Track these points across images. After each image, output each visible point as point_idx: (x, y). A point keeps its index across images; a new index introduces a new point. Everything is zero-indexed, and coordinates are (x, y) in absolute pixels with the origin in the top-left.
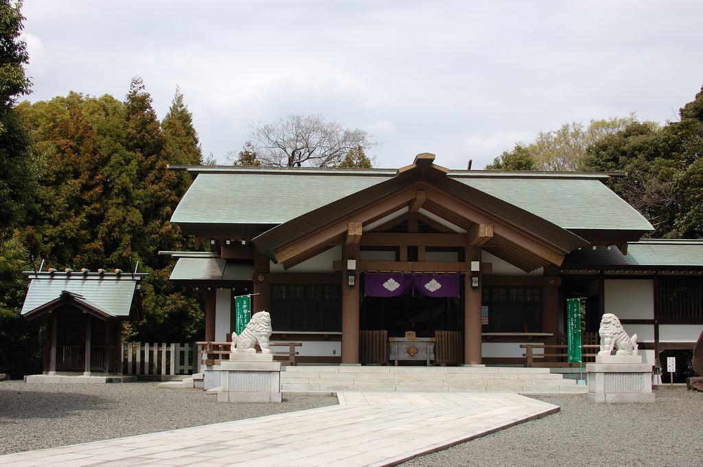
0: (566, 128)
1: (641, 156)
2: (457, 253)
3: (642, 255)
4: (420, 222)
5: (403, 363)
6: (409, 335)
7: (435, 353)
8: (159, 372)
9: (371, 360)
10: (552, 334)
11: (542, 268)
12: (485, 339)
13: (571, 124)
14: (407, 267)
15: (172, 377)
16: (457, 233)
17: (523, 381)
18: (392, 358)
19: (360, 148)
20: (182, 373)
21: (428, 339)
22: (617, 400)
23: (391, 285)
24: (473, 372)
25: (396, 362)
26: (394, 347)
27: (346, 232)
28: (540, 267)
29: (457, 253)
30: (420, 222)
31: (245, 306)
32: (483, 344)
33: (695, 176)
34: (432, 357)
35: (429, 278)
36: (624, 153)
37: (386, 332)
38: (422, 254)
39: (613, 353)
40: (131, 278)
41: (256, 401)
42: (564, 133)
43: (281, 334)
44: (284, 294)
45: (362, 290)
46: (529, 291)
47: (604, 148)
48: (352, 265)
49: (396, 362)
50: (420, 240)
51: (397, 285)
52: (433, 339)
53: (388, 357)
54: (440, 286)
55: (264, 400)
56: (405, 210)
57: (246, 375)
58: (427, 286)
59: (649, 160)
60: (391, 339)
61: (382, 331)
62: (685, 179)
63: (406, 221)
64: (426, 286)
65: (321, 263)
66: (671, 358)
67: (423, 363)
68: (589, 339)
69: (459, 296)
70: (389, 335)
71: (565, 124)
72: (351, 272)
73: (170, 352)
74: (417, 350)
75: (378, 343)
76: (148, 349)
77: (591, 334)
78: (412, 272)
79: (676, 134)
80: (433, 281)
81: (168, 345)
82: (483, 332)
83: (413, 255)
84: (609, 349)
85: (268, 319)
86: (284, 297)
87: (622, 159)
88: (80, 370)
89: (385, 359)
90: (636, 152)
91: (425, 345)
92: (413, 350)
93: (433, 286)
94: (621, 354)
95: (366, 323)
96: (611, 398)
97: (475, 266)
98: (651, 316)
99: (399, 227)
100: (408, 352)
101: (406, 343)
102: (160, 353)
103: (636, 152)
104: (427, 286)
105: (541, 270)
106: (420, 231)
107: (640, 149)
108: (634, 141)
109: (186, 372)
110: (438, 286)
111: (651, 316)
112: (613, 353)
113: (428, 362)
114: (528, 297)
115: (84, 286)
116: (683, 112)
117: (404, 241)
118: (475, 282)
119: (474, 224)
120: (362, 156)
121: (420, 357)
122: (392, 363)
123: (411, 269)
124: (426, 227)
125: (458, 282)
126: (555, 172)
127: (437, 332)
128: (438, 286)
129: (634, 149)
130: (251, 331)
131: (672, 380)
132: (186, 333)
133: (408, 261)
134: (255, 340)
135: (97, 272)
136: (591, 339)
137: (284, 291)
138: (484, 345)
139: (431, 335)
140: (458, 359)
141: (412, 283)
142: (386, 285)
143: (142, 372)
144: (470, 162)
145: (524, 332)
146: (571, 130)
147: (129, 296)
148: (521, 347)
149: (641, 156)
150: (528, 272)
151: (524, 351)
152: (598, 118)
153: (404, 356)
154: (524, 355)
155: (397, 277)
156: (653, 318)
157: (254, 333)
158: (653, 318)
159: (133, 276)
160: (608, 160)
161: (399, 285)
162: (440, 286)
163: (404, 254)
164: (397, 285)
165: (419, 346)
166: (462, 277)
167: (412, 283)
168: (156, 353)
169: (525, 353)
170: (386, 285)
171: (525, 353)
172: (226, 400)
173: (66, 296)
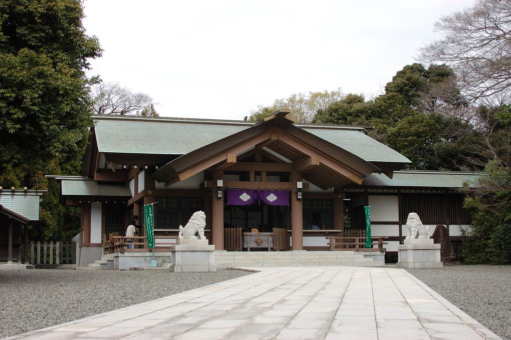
0: (294, 96)
1: (363, 117)
2: (279, 177)
3: (400, 180)
5: (252, 250)
6: (254, 231)
7: (273, 243)
8: (54, 263)
9: (229, 248)
10: (341, 231)
11: (333, 188)
12: (305, 234)
13: (298, 94)
15: (57, 265)
16: (286, 163)
18: (245, 246)
19: (152, 105)
20: (65, 262)
21: (269, 233)
22: (421, 266)
23: (245, 197)
24: (298, 254)
25: (249, 249)
26: (247, 239)
29: (279, 177)
31: (150, 211)
32: (304, 238)
33: (404, 130)
34: (272, 245)
35: (269, 192)
36: (350, 114)
37: (241, 229)
39: (417, 237)
40: (35, 194)
41: (200, 271)
43: (164, 231)
45: (225, 201)
47: (336, 111)
49: (249, 249)
51: (249, 197)
52: (272, 233)
53: (243, 245)
54: (276, 198)
55: (205, 271)
57: (192, 253)
58: (268, 198)
59: (368, 120)
60: (245, 233)
61: (238, 229)
62: (397, 132)
67: (265, 249)
68: (353, 233)
69: (288, 205)
70: (243, 231)
71: (293, 94)
73: (55, 247)
74: (262, 241)
75: (235, 237)
76: (40, 246)
77: (361, 230)
78: (258, 189)
79: (386, 102)
80: (272, 195)
81: (55, 243)
82: (303, 229)
84: (414, 235)
85: (205, 216)
86: (164, 206)
87: (349, 118)
89: (241, 247)
90: (360, 114)
92: (259, 242)
93: (272, 198)
94: (421, 238)
96: (417, 265)
97: (300, 185)
98: (397, 220)
100: (256, 242)
101: (254, 236)
102: (48, 248)
103: (360, 114)
104: (268, 198)
107: (362, 112)
108: (357, 106)
109: (68, 262)
110: (275, 198)
111: (397, 220)
112: (417, 237)
113: (269, 249)
114: (324, 207)
116: (387, 89)
120: (153, 112)
121: (264, 245)
122: (245, 250)
125: (286, 195)
127: (274, 229)
128: (275, 198)
129: (358, 111)
132: (45, 236)
136: (355, 233)
137: (164, 202)
138: (305, 238)
139: (271, 231)
140: (287, 247)
142: (241, 197)
143: (48, 262)
145: (333, 229)
146: (298, 98)
147: (36, 206)
149: (363, 117)
150: (325, 190)
151: (328, 241)
152: (315, 91)
153: (254, 245)
154: (328, 244)
155: (276, 192)
156: (398, 221)
158: (398, 221)
159: (37, 192)
160: (339, 119)
162: (276, 198)
164: (249, 197)
165: (263, 238)
166: (290, 192)
168: (45, 248)
169: (329, 242)
170: (241, 197)
171: (329, 242)
172: (180, 271)
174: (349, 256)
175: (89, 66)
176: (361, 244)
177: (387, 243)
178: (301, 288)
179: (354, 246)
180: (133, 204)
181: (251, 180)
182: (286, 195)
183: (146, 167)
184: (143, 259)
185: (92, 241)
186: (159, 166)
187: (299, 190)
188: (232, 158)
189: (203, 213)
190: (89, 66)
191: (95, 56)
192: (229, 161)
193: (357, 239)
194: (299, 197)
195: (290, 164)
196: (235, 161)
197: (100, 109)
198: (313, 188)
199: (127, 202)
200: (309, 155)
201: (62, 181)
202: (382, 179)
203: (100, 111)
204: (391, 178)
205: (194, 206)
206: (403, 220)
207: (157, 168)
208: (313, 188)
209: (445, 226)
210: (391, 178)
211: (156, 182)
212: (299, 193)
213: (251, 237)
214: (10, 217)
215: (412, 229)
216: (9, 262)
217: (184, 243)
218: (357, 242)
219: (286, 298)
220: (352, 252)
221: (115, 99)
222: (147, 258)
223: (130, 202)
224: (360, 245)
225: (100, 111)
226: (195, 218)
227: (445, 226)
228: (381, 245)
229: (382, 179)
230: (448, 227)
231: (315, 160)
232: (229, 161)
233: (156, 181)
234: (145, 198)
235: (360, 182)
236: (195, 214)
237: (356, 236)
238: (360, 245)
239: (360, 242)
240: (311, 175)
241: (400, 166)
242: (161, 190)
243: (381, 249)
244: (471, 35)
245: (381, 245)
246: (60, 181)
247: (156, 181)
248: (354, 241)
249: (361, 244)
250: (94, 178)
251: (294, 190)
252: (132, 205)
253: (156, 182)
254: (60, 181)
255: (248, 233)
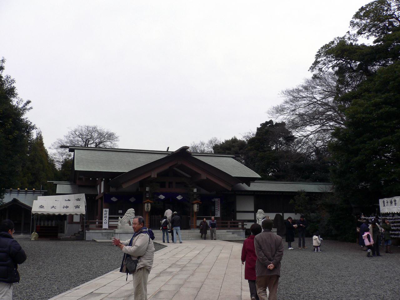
3: (254, 187)
27: (151, 176)
32: (197, 221)
42: (44, 144)
72: (147, 192)
85: (134, 212)
93: (179, 198)
97: (195, 190)
98: (253, 209)
115: (19, 196)
118: (148, 195)
119: (199, 174)
126: (202, 153)
130: (127, 216)
131: (110, 216)
134: (129, 220)
135: (17, 189)
144: (168, 148)
157: (128, 218)
159: (41, 192)
173: (15, 200)
174: (224, 233)
175: (310, 71)
177: (246, 225)
178: (194, 250)
179: (227, 227)
180: (98, 199)
183: (104, 179)
184: (100, 234)
185: (74, 221)
186: (111, 178)
188: (154, 175)
189: (133, 209)
190: (310, 71)
192: (152, 176)
193: (229, 222)
196: (156, 176)
197: (86, 141)
198: (204, 192)
199: (95, 197)
200: (200, 173)
201: (58, 185)
202: (245, 186)
203: (86, 141)
204: (249, 186)
206: (255, 212)
207: (110, 179)
208: (204, 192)
209: (281, 214)
210: (249, 186)
211: (111, 188)
215: (260, 219)
216: (21, 234)
217: (121, 228)
218: (229, 224)
219: (163, 289)
221: (95, 135)
222: (104, 234)
223: (97, 198)
225: (86, 141)
226: (128, 213)
227: (281, 214)
228: (243, 225)
229: (245, 186)
230: (283, 215)
231: (204, 176)
232: (152, 176)
233: (111, 187)
234: (99, 199)
235: (230, 189)
236: (129, 210)
240: (201, 184)
241: (253, 180)
243: (243, 228)
244: (170, 277)
245: (243, 225)
246: (56, 184)
247: (111, 187)
248: (227, 223)
250: (76, 183)
252: (98, 200)
254: (56, 184)
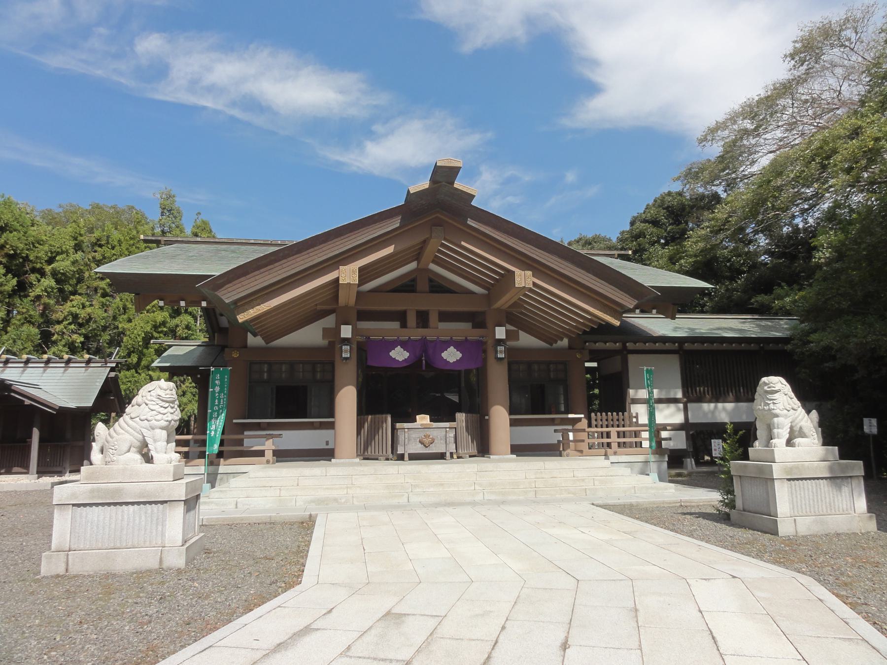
4: (431, 280)
5: (414, 457)
14: (415, 334)
17: (583, 480)
18: (400, 451)
21: (447, 424)
23: (399, 355)
27: (337, 279)
28: (562, 339)
30: (431, 280)
35: (446, 345)
38: (433, 318)
43: (313, 422)
44: (266, 374)
46: (552, 367)
48: (346, 331)
50: (434, 304)
51: (406, 355)
52: (453, 424)
56: (413, 265)
60: (398, 425)
63: (414, 280)
64: (443, 355)
65: (310, 336)
66: (717, 441)
67: (441, 456)
68: (618, 420)
72: (346, 341)
83: (423, 319)
88: (23, 466)
91: (443, 432)
93: (451, 355)
95: (368, 406)
99: (406, 286)
100: (421, 442)
104: (445, 355)
105: (565, 342)
106: (432, 292)
117: (410, 304)
118: (501, 352)
123: (419, 338)
124: (438, 287)
125: (476, 350)
128: (459, 355)
133: (417, 327)
140: (484, 449)
141: (424, 352)
142: (393, 354)
145: (544, 414)
148: (556, 431)
153: (419, 449)
155: (405, 345)
161: (408, 354)
163: (412, 320)
164: (406, 355)
165: (434, 433)
167: (424, 352)
170: (393, 354)
176: (622, 440)
181: (409, 325)
182: (476, 350)
187: (500, 342)
191: (798, 45)
193: (613, 431)
194: (499, 356)
195: (483, 295)
198: (526, 340)
205: (319, 376)
208: (526, 340)
211: (249, 335)
212: (499, 348)
213: (412, 432)
214: (27, 402)
218: (614, 438)
220: (599, 462)
224: (619, 443)
235: (617, 323)
237: (613, 426)
238: (619, 443)
239: (618, 437)
242: (257, 349)
248: (608, 435)
249: (622, 440)
251: (490, 342)
253: (249, 335)
255: (406, 425)
